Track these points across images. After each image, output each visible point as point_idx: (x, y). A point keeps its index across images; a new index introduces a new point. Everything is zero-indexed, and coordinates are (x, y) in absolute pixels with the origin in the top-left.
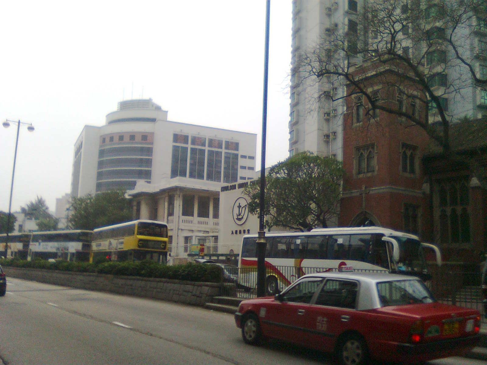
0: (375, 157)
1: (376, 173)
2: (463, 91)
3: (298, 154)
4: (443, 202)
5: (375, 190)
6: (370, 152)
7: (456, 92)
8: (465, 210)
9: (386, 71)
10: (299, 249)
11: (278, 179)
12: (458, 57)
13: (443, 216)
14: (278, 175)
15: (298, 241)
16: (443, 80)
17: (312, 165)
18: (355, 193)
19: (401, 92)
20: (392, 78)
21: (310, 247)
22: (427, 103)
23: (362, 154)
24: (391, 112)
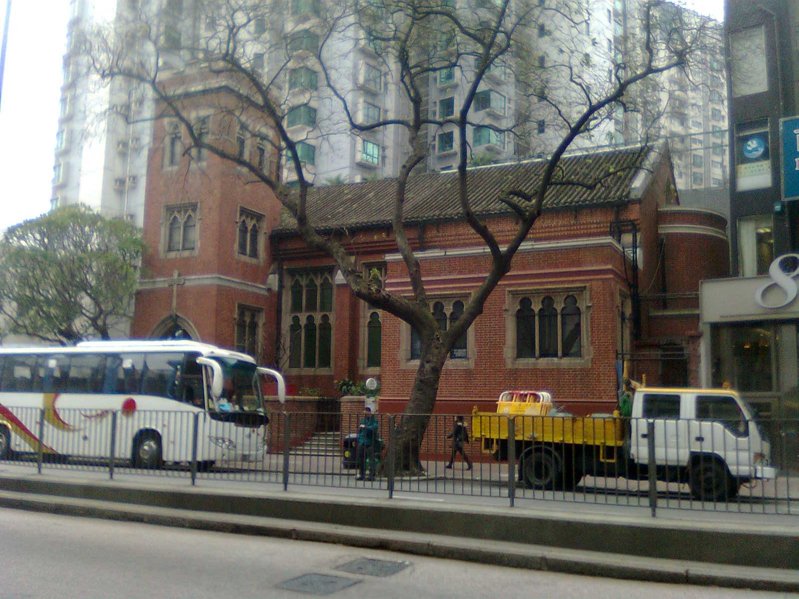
0: (196, 226)
1: (196, 253)
2: (333, 138)
3: (63, 208)
4: (296, 307)
5: (195, 280)
6: (190, 216)
7: (323, 139)
8: (325, 318)
9: (219, 89)
10: (52, 377)
11: (21, 249)
12: (329, 85)
13: (295, 327)
14: (23, 243)
15: (52, 363)
16: (311, 117)
17: (87, 229)
18: (161, 283)
19: (244, 127)
20: (229, 101)
21: (73, 373)
22: (280, 149)
23: (190, 216)
24: (223, 155)
